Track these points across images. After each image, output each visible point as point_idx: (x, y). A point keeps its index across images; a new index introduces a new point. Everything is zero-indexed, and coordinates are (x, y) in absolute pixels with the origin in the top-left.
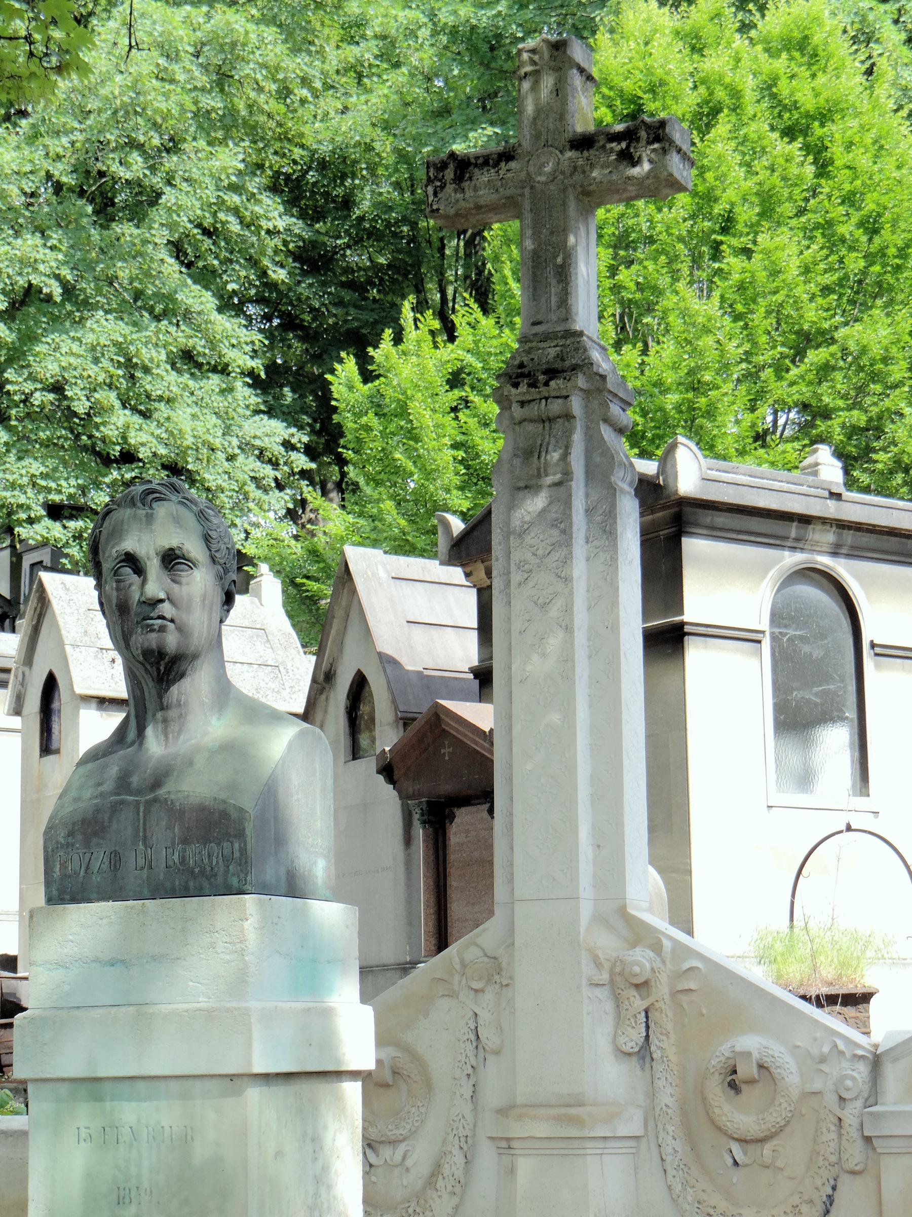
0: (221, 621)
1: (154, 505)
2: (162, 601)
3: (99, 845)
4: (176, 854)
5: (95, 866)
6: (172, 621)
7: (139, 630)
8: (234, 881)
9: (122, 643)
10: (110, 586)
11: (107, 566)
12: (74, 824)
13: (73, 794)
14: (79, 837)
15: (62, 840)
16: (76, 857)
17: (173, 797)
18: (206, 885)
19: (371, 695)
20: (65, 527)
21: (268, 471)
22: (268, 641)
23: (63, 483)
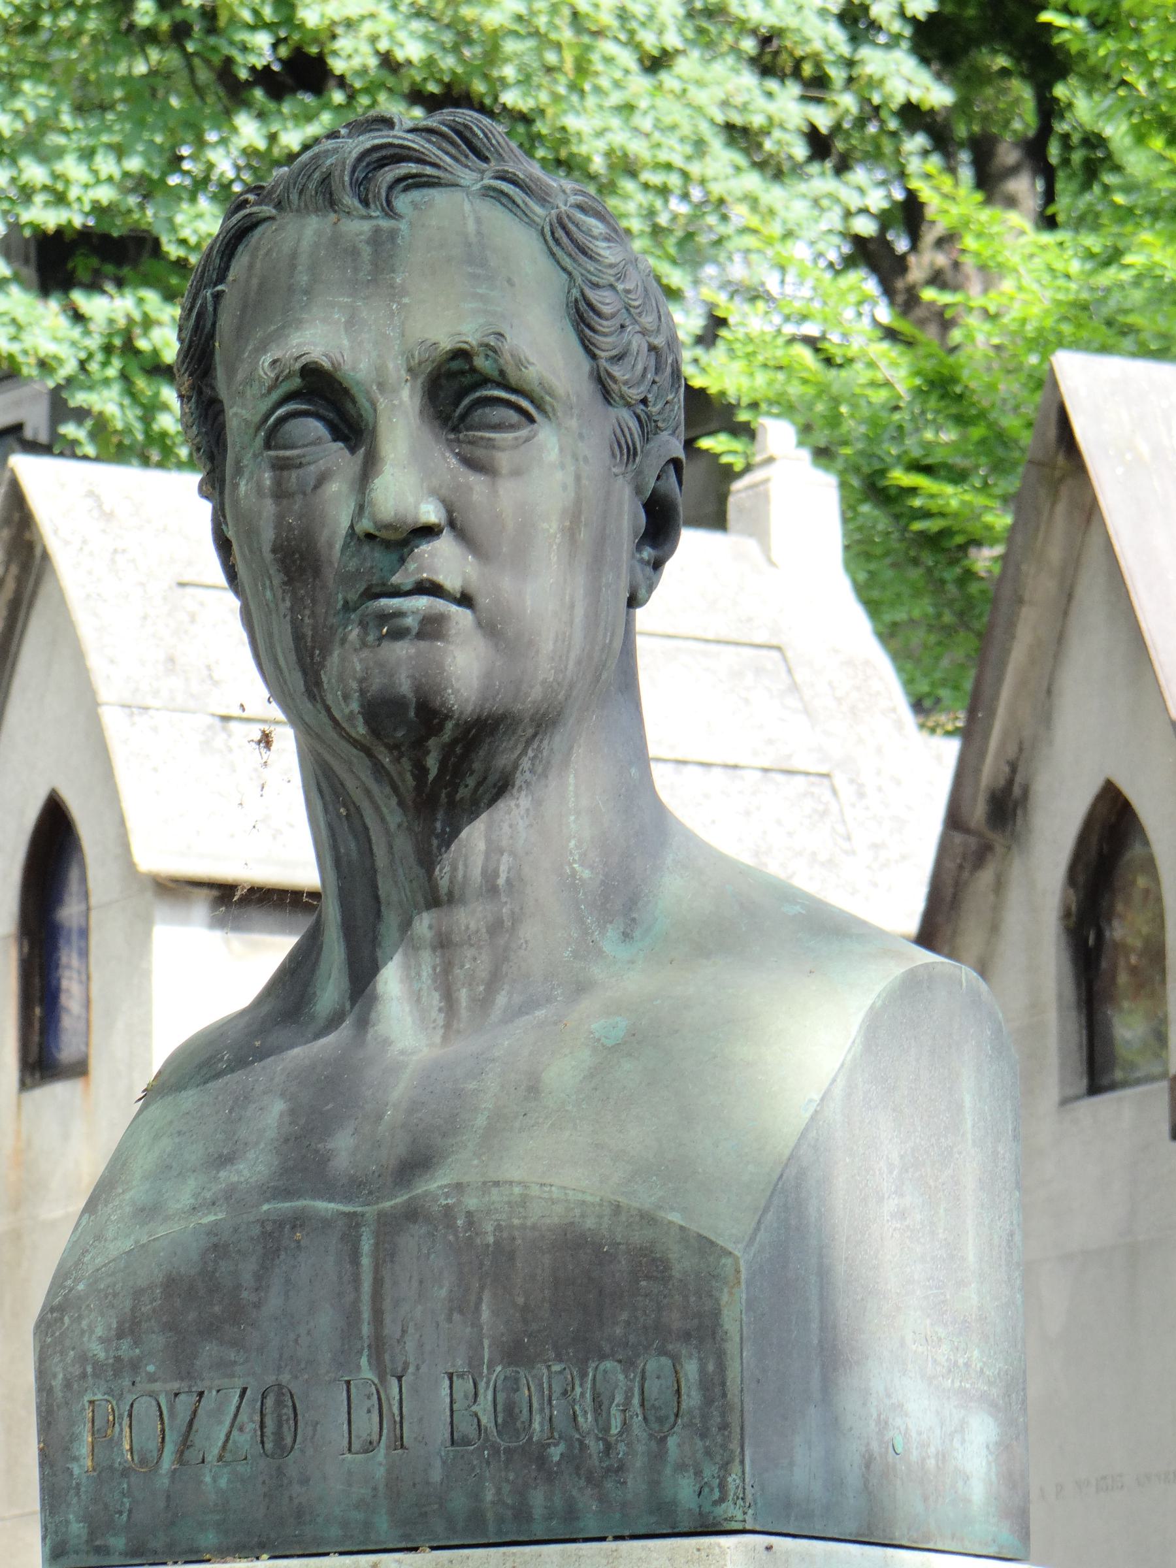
0: (633, 602)
1: (402, 202)
2: (428, 532)
4: (486, 1398)
5: (212, 1437)
6: (465, 600)
7: (354, 633)
8: (684, 1491)
9: (296, 681)
10: (252, 483)
11: (241, 414)
12: (138, 1294)
13: (135, 1191)
14: (157, 1341)
15: (98, 1350)
16: (145, 1407)
17: (472, 1202)
18: (588, 1502)
19: (1149, 866)
20: (78, 317)
21: (786, 110)
22: (794, 687)
23: (72, 167)
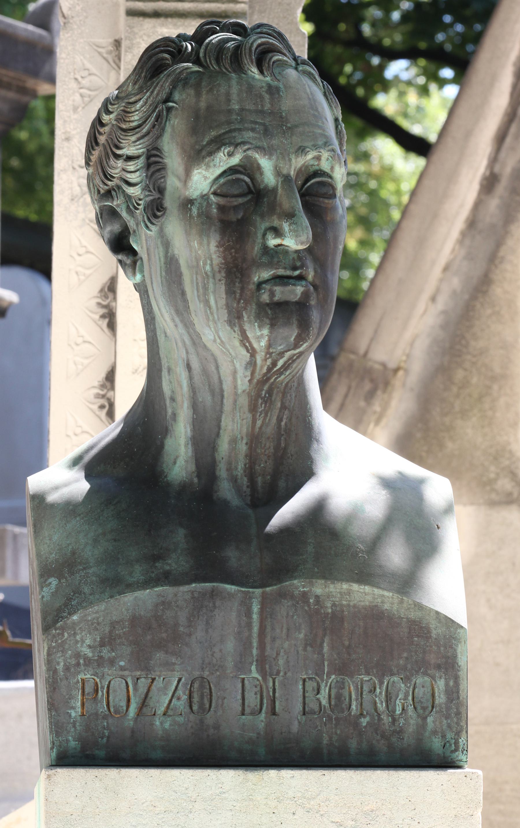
3: (169, 666)
8: (436, 744)
12: (113, 625)
14: (126, 650)
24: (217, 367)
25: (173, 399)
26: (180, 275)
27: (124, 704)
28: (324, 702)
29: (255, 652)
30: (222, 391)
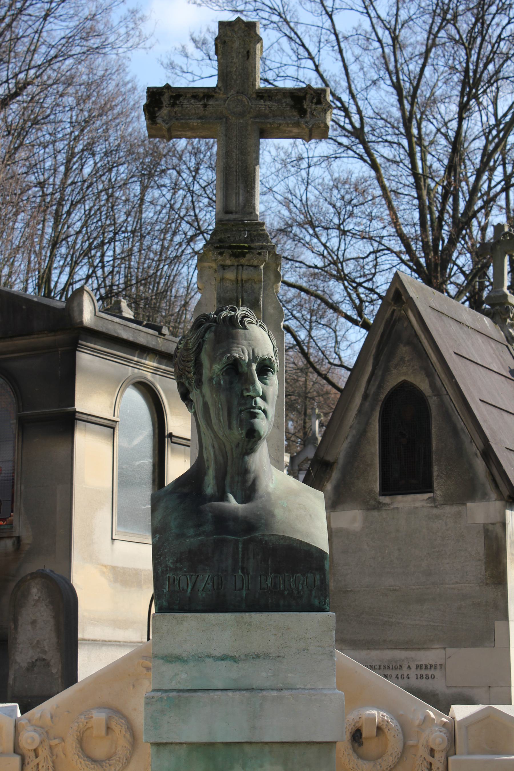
8: (316, 602)
17: (266, 538)
24: (225, 447)
25: (207, 460)
26: (209, 408)
27: (185, 587)
28: (269, 585)
29: (240, 564)
30: (227, 456)
